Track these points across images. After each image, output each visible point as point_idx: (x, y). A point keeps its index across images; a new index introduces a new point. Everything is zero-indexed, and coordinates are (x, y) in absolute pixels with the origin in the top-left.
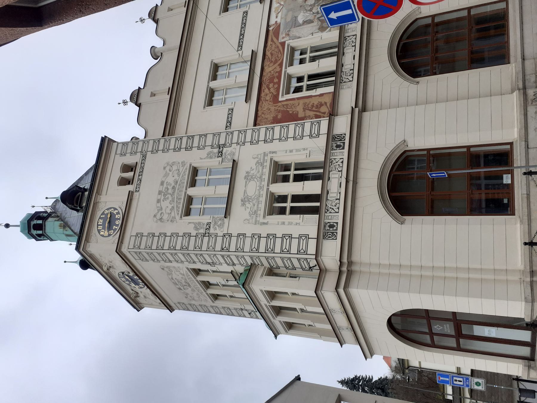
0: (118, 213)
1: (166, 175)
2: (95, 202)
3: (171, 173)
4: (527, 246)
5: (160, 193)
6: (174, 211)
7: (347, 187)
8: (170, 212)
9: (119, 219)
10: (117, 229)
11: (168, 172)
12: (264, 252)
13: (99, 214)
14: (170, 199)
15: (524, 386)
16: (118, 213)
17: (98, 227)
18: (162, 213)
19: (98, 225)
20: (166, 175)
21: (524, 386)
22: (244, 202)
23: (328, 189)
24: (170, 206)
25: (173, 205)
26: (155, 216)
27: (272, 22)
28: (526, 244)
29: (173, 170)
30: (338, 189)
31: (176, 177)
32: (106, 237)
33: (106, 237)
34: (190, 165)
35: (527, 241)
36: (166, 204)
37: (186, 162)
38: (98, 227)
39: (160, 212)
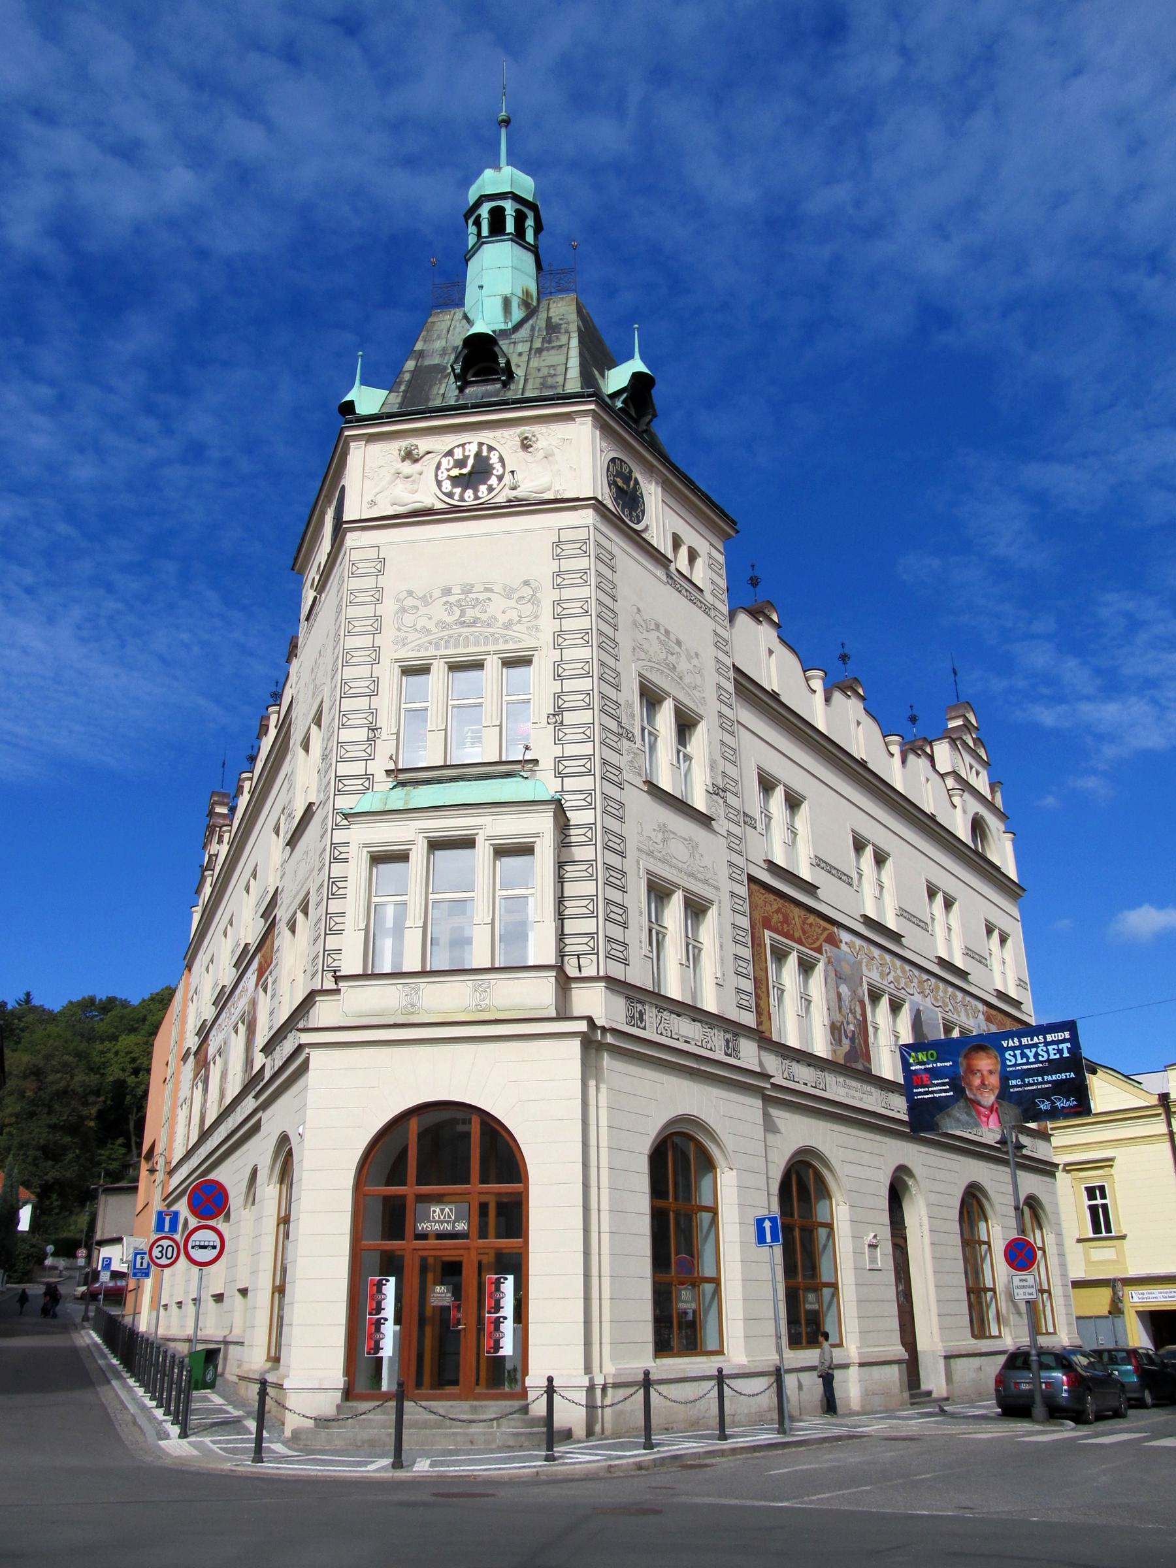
0: (491, 489)
1: (508, 593)
2: (573, 414)
3: (512, 603)
4: (546, 1383)
5: (468, 589)
6: (420, 638)
7: (525, 1038)
8: (418, 627)
9: (477, 498)
10: (452, 498)
11: (517, 595)
12: (331, 876)
13: (488, 437)
14: (450, 619)
15: (537, 1398)
16: (491, 489)
17: (458, 446)
18: (416, 607)
19: (463, 445)
20: (508, 593)
21: (537, 1398)
22: (663, 828)
23: (683, 1016)
24: (431, 625)
25: (434, 630)
26: (410, 593)
27: (845, 936)
28: (550, 1380)
29: (518, 607)
30: (684, 1037)
31: (503, 619)
32: (436, 475)
33: (436, 475)
34: (535, 649)
35: (555, 1383)
36: (438, 611)
37: (538, 635)
38: (458, 446)
39: (418, 603)
